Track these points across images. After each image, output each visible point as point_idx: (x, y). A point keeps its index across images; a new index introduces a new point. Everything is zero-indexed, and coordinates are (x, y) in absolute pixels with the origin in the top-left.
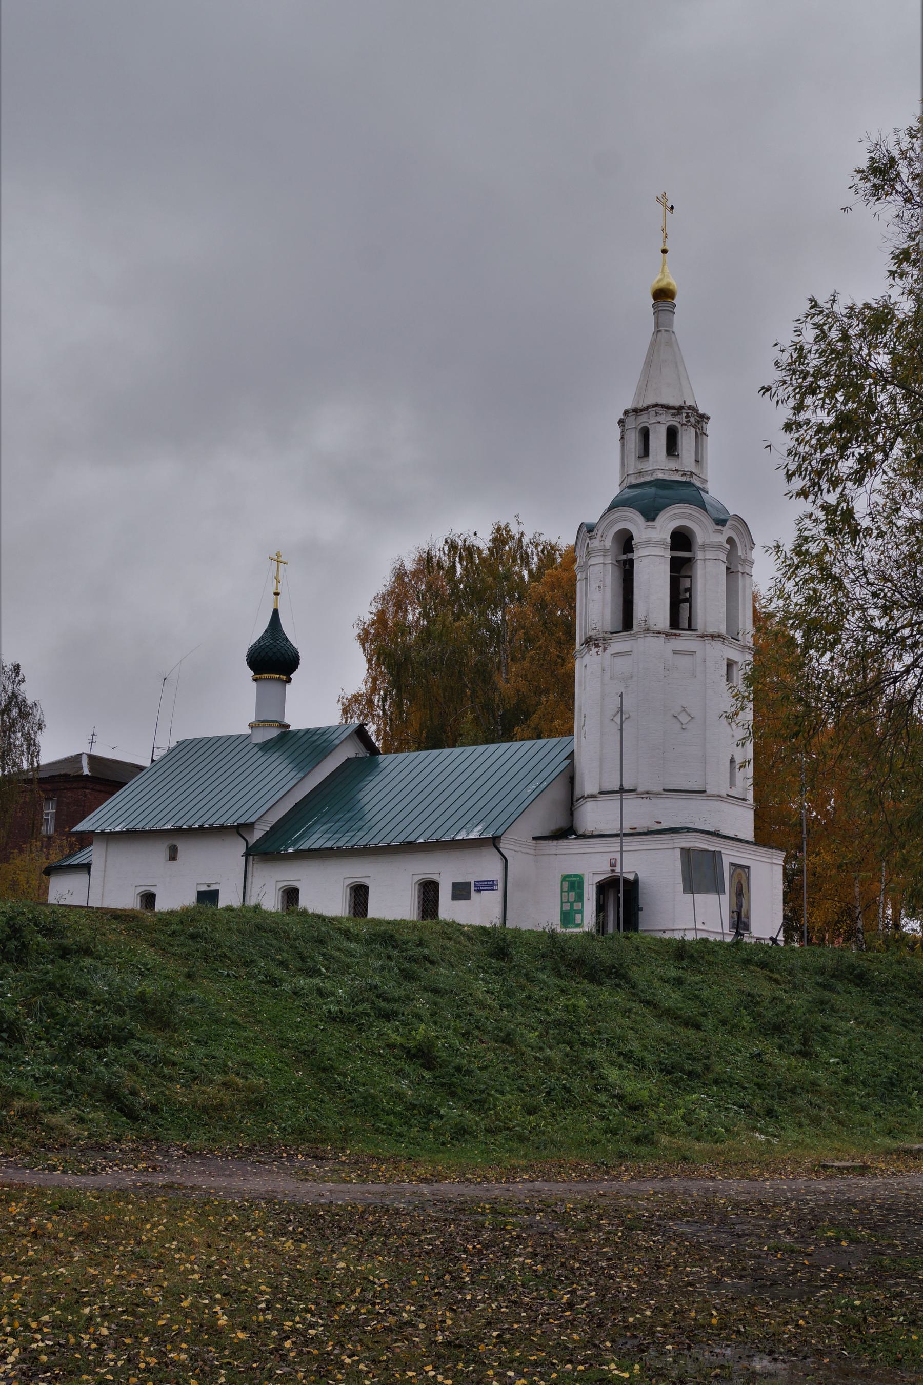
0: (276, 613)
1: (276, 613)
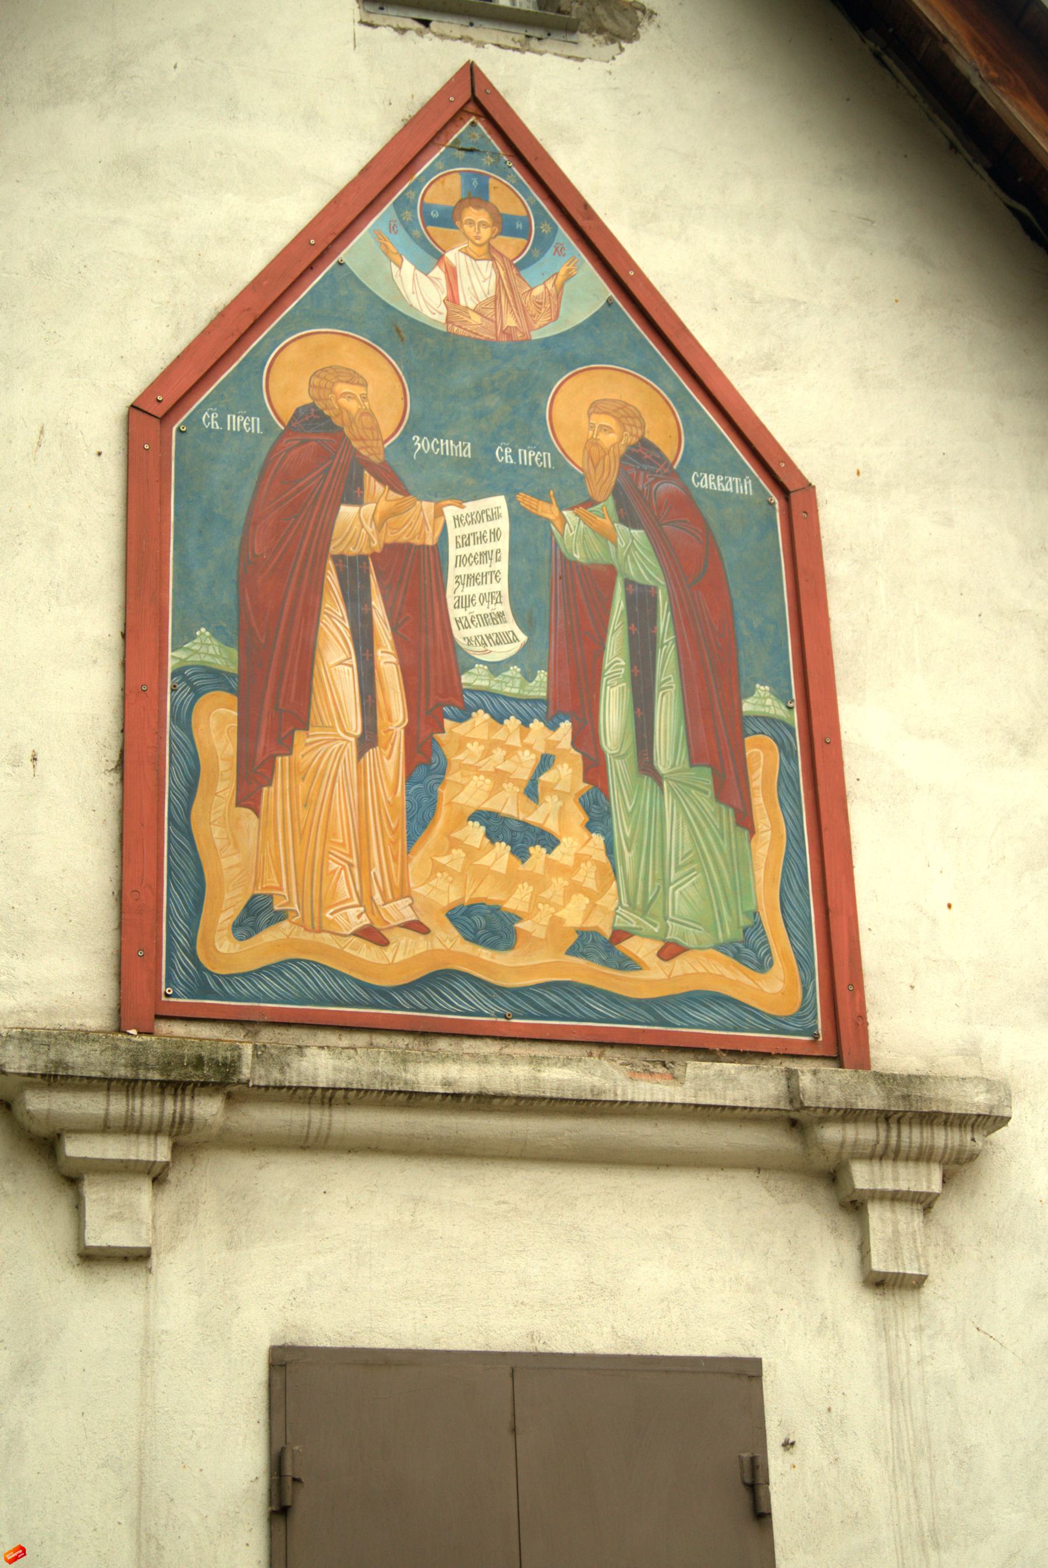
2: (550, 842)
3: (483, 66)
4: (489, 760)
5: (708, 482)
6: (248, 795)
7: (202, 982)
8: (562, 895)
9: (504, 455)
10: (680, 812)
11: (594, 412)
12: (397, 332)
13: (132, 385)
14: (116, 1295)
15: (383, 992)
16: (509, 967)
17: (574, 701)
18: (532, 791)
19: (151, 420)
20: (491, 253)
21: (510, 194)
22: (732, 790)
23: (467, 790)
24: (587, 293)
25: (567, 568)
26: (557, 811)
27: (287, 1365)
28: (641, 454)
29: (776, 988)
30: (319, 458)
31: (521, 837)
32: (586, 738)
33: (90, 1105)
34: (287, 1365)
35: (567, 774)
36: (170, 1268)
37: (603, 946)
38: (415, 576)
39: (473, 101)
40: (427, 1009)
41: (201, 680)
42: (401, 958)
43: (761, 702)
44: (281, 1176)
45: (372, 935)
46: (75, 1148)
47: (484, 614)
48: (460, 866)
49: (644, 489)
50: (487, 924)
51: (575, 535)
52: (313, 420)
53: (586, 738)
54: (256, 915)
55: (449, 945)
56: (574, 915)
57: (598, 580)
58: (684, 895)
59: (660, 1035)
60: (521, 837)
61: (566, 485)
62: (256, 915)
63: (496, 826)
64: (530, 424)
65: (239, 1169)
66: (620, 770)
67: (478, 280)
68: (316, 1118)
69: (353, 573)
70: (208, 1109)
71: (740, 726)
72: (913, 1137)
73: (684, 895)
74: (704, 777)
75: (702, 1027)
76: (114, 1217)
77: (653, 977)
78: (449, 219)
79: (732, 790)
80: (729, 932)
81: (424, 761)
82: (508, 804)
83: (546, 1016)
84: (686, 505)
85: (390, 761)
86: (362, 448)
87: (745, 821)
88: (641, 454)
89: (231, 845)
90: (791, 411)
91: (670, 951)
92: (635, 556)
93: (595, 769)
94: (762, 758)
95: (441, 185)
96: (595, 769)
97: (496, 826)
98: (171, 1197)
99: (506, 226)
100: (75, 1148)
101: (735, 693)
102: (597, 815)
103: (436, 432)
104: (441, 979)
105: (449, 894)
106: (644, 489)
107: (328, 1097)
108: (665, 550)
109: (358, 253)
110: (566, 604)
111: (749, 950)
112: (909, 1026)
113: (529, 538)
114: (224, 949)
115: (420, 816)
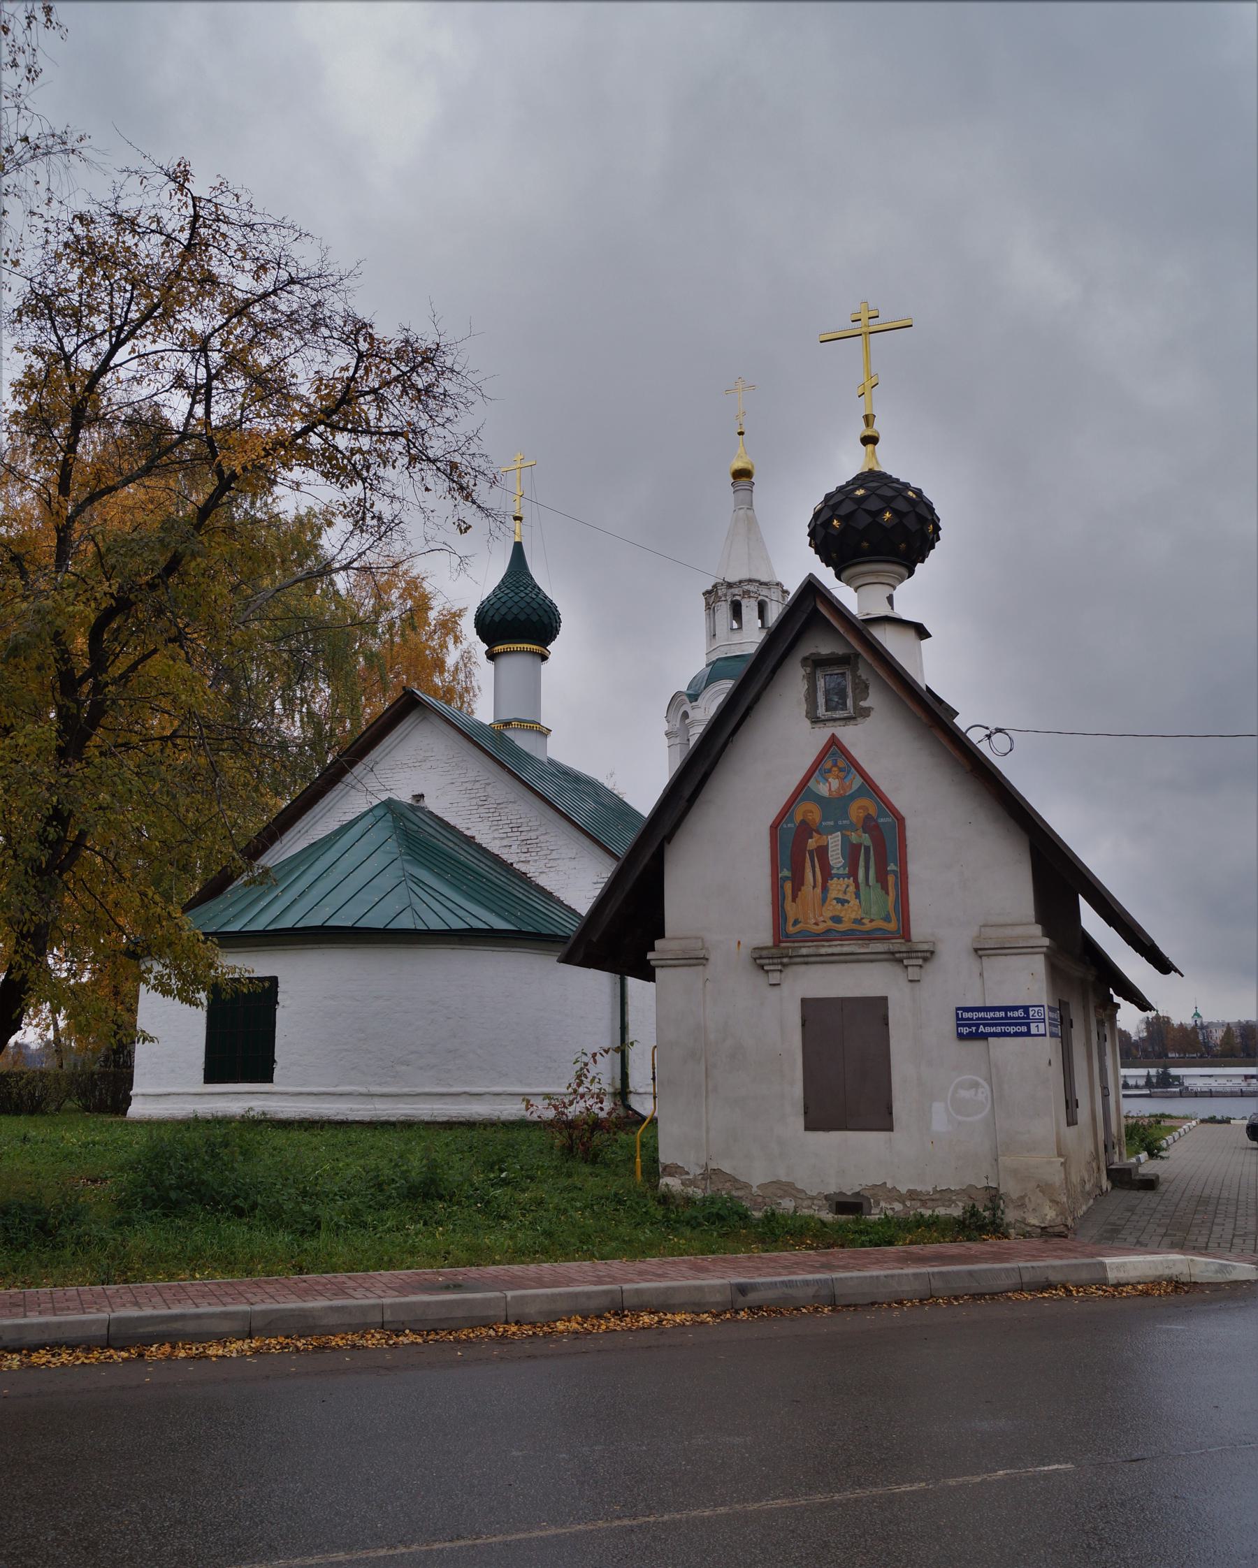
0: (518, 547)
1: (518, 547)
2: (848, 902)
3: (839, 735)
4: (837, 887)
5: (881, 820)
6: (794, 900)
7: (787, 936)
8: (851, 912)
9: (840, 823)
10: (875, 893)
11: (856, 811)
12: (819, 799)
13: (770, 822)
14: (776, 990)
15: (818, 935)
16: (841, 927)
17: (853, 873)
18: (845, 893)
19: (774, 827)
20: (838, 777)
21: (842, 763)
22: (885, 887)
23: (833, 893)
24: (858, 781)
25: (853, 845)
26: (850, 896)
27: (804, 1001)
28: (868, 817)
29: (892, 926)
30: (806, 830)
31: (842, 902)
32: (856, 881)
33: (767, 961)
34: (804, 1001)
35: (852, 888)
36: (785, 986)
37: (859, 921)
38: (822, 852)
39: (834, 741)
40: (826, 936)
41: (785, 879)
42: (822, 927)
43: (891, 867)
44: (803, 968)
45: (816, 924)
46: (906, 962)
47: (836, 858)
48: (832, 908)
49: (869, 825)
50: (836, 919)
51: (854, 838)
52: (803, 822)
53: (856, 881)
54: (796, 922)
55: (830, 923)
56: (853, 916)
57: (859, 846)
58: (874, 909)
59: (869, 937)
60: (842, 902)
61: (852, 827)
62: (796, 922)
63: (838, 900)
64: (845, 814)
65: (795, 968)
66: (862, 886)
67: (835, 784)
68: (806, 959)
69: (811, 853)
70: (785, 960)
71: (887, 873)
72: (914, 955)
73: (874, 909)
74: (879, 885)
75: (878, 935)
76: (774, 978)
77: (868, 926)
78: (830, 771)
79: (885, 887)
80: (883, 915)
81: (825, 888)
82: (841, 896)
83: (848, 935)
84: (877, 826)
85: (818, 890)
86: (762, 614)
87: (887, 893)
88: (868, 817)
89: (790, 908)
90: (900, 801)
91: (871, 921)
92: (866, 839)
93: (857, 886)
94: (891, 879)
95: (828, 764)
96: (857, 886)
97: (838, 900)
98: (783, 974)
99: (841, 770)
100: (906, 962)
101: (886, 865)
102: (857, 896)
103: (826, 820)
104: (828, 931)
105: (829, 914)
106: (869, 825)
107: (807, 956)
108: (872, 837)
109: (811, 784)
110: (852, 853)
111: (887, 919)
112: (920, 930)
113: (845, 839)
114: (791, 929)
115: (824, 900)
